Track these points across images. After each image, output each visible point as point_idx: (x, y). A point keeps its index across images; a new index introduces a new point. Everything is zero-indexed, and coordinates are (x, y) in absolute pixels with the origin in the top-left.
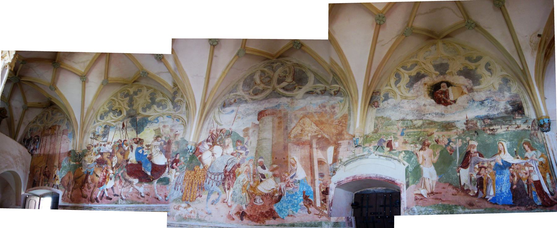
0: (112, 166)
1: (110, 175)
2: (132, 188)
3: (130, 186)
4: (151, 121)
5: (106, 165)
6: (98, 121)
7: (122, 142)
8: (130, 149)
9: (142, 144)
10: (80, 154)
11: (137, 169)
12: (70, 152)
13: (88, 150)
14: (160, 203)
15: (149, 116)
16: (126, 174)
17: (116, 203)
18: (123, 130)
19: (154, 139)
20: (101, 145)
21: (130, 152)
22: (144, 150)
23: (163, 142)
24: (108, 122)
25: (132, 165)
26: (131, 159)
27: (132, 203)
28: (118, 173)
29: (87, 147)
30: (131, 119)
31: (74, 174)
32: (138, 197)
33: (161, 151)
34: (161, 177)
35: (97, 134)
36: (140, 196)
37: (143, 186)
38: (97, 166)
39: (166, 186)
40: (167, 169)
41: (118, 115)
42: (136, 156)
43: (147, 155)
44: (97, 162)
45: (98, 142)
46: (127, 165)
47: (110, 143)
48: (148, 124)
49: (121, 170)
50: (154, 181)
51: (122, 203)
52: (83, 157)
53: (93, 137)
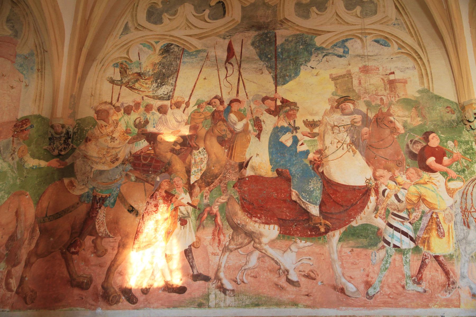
0: (189, 180)
1: (182, 208)
2: (256, 254)
3: (250, 247)
4: (323, 49)
5: (166, 174)
6: (139, 27)
7: (226, 104)
8: (250, 128)
9: (290, 116)
10: (68, 133)
11: (275, 195)
12: (25, 121)
13: (101, 122)
14: (348, 305)
15: (318, 33)
16: (238, 208)
17: (200, 305)
18: (229, 67)
19: (332, 107)
20: (148, 108)
21: (253, 139)
22: (299, 136)
23: (358, 118)
24: (175, 33)
25: (257, 179)
26: (255, 162)
27: (257, 305)
28: (208, 205)
29: (97, 112)
30: (257, 33)
31: (37, 203)
32: (277, 285)
33: (353, 143)
34: (354, 224)
35: (137, 70)
36: (283, 282)
37: (293, 248)
38: (133, 178)
39: (369, 251)
40: (373, 198)
41: (214, 17)
42: (271, 154)
43: (307, 153)
44: (134, 165)
45: (139, 99)
46: (241, 180)
47: (184, 105)
48: (313, 58)
49: (221, 195)
50: (330, 233)
51: (222, 304)
52: (78, 145)
53: (118, 77)
